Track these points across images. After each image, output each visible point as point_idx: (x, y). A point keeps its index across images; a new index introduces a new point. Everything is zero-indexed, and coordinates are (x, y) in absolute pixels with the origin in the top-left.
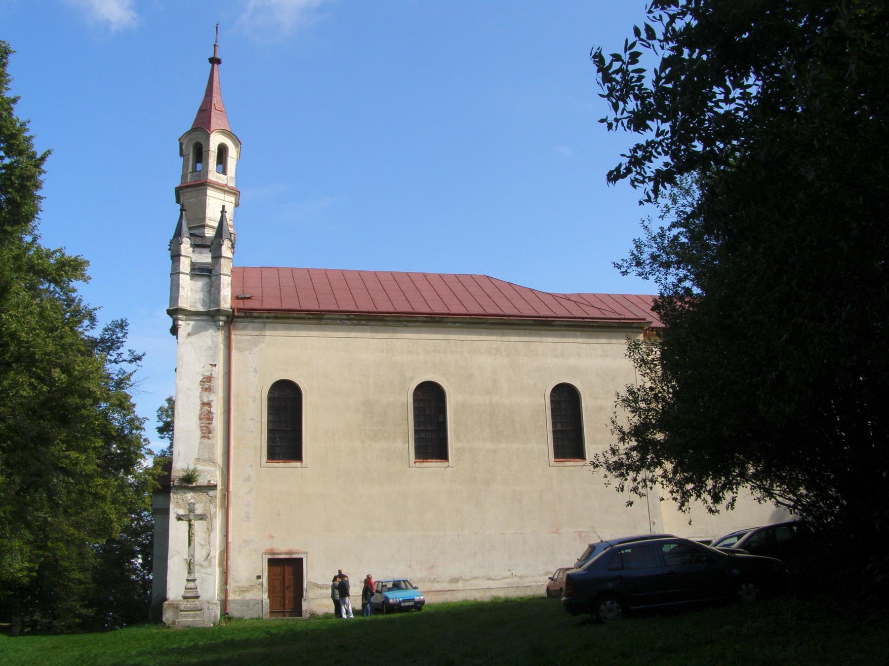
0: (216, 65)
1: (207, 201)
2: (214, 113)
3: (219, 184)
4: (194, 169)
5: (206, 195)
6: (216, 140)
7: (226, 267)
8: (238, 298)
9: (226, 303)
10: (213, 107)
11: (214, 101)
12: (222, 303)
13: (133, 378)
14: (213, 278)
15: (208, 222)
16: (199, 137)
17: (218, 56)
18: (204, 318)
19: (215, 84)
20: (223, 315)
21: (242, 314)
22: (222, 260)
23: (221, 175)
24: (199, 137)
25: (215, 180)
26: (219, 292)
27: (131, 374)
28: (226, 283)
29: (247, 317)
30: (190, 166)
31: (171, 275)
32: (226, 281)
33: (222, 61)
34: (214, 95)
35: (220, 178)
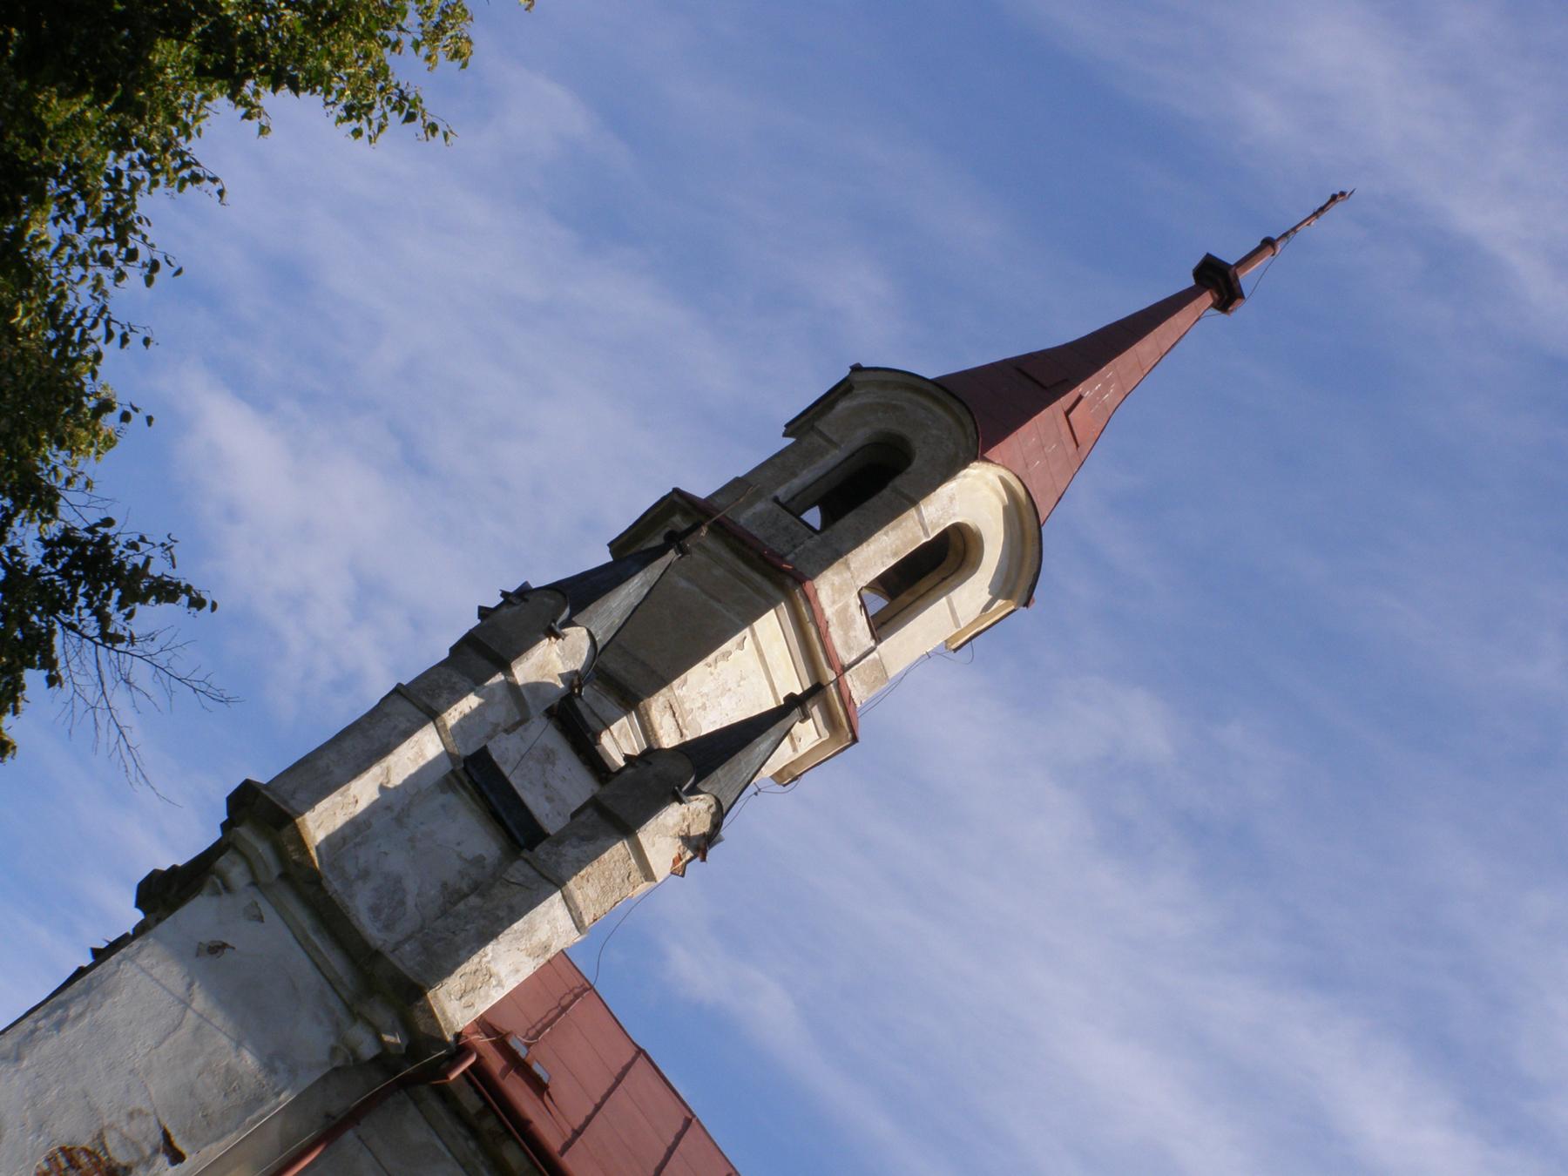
0: (1207, 299)
1: (729, 645)
2: (1048, 419)
3: (823, 637)
4: (794, 507)
5: (749, 616)
6: (973, 497)
7: (601, 882)
8: (501, 1043)
9: (478, 990)
10: (1065, 401)
11: (1088, 389)
12: (454, 983)
13: (150, 616)
14: (518, 871)
15: (657, 706)
16: (931, 429)
17: (1246, 278)
18: (336, 961)
19: (1145, 348)
20: (407, 1026)
21: (470, 1101)
22: (620, 849)
23: (861, 621)
24: (931, 429)
25: (830, 611)
26: (488, 934)
27: (167, 591)
28: (542, 934)
29: (474, 1133)
30: (796, 483)
31: (398, 691)
32: (549, 926)
33: (1241, 310)
34: (1108, 371)
35: (846, 624)
